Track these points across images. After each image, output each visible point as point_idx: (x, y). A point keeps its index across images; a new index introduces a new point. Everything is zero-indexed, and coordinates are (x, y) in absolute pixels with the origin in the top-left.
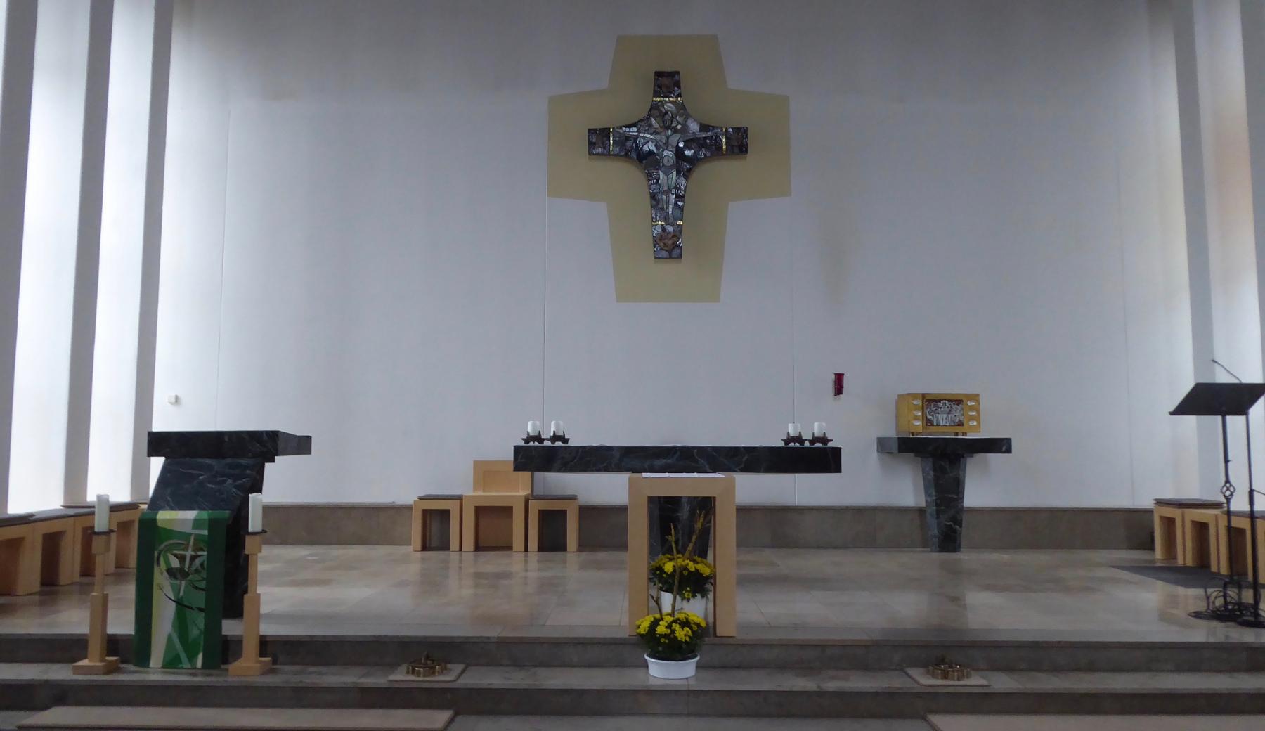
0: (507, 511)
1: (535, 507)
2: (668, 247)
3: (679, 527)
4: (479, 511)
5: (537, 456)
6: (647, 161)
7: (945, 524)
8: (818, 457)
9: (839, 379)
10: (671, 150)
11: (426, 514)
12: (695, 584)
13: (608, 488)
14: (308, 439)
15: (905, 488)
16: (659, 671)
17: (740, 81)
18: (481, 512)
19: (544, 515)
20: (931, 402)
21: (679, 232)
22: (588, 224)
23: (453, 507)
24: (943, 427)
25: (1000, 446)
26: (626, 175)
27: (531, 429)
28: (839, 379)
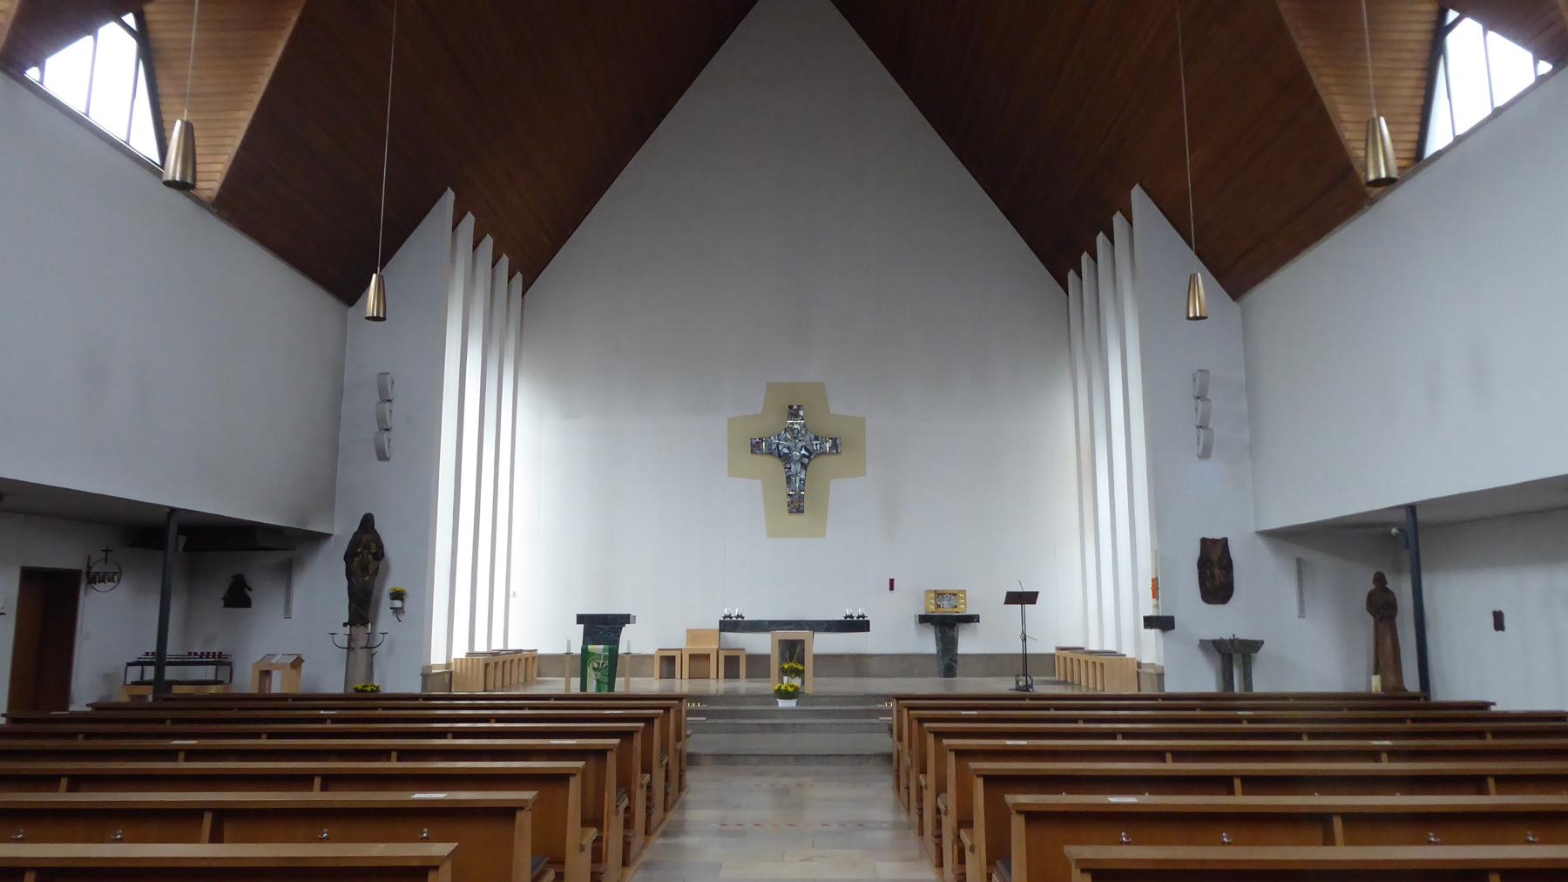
2: (796, 506)
3: (792, 650)
4: (691, 656)
5: (728, 625)
6: (785, 459)
7: (948, 660)
8: (858, 625)
9: (892, 581)
10: (797, 456)
11: (662, 658)
12: (799, 673)
13: (761, 644)
14: (1146, 626)
15: (927, 644)
17: (839, 407)
18: (694, 657)
19: (726, 658)
20: (939, 595)
21: (801, 498)
22: (752, 494)
23: (677, 655)
24: (947, 609)
25: (972, 619)
26: (775, 465)
27: (726, 612)
28: (892, 581)
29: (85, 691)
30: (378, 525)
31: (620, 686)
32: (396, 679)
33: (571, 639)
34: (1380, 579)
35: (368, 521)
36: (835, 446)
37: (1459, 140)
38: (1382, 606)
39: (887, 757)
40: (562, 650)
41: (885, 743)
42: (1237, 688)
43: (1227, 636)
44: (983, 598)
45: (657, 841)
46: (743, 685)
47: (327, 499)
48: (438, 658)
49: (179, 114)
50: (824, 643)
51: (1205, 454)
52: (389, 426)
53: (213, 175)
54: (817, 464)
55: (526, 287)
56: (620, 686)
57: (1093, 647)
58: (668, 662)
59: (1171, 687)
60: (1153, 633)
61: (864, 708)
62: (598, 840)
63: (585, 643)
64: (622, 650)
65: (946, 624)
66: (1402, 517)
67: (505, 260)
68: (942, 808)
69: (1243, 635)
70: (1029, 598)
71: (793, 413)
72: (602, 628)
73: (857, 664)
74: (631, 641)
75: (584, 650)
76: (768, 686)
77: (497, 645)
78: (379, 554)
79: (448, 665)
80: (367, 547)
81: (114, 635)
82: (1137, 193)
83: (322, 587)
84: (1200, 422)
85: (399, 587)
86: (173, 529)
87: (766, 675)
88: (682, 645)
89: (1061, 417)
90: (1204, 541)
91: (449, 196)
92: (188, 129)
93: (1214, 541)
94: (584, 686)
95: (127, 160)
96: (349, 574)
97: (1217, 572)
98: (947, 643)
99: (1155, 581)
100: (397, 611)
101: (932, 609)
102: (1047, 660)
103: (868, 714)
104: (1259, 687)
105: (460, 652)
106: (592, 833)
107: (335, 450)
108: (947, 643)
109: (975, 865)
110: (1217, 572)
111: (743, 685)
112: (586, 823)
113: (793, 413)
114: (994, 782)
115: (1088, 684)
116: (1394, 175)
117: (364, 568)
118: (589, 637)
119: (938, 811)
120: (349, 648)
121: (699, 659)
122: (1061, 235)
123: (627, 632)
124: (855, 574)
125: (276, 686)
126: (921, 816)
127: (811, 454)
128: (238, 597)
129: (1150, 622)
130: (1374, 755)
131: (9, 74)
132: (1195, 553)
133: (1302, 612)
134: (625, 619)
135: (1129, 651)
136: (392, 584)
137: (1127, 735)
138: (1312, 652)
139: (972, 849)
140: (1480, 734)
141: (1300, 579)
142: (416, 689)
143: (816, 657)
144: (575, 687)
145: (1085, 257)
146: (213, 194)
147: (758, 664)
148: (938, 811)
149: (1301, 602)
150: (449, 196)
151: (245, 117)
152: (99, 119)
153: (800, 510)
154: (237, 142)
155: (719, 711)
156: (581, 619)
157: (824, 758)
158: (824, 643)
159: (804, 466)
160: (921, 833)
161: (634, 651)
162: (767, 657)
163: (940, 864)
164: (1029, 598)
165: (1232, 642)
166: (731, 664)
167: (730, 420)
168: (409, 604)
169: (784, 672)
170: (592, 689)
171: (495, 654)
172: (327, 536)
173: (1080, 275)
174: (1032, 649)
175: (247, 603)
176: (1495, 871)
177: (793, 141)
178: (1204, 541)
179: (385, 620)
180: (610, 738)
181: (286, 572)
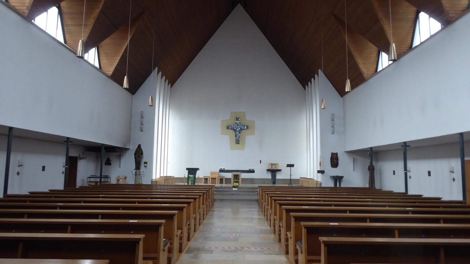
0: (215, 178)
1: (219, 178)
2: (238, 142)
3: (236, 177)
5: (221, 171)
6: (235, 131)
7: (274, 180)
8: (252, 171)
9: (394, 174)
10: (238, 130)
12: (238, 182)
13: (229, 175)
15: (269, 176)
16: (234, 189)
17: (249, 118)
19: (220, 179)
20: (272, 164)
22: (226, 139)
24: (274, 168)
25: (280, 170)
26: (232, 132)
28: (394, 174)
29: (79, 184)
30: (142, 147)
31: (196, 184)
32: (146, 181)
33: (185, 174)
34: (371, 163)
35: (139, 146)
36: (247, 128)
37: (422, 43)
38: (371, 169)
39: (257, 200)
40: (183, 177)
41: (257, 197)
42: (338, 186)
43: (336, 175)
44: (282, 165)
45: (210, 212)
46: (224, 185)
47: (129, 139)
48: (154, 178)
49: (81, 39)
50: (243, 176)
51: (333, 133)
52: (141, 124)
53: (110, 70)
54: (243, 131)
55: (171, 87)
56: (196, 184)
57: (309, 177)
58: (206, 179)
59: (323, 186)
60: (320, 174)
61: (253, 190)
62: (182, 233)
63: (188, 175)
64: (197, 177)
65: (274, 171)
66: (369, 149)
67: (167, 81)
68: (281, 226)
69: (339, 175)
70: (292, 166)
71: (237, 119)
72: (192, 171)
73: (252, 181)
74: (199, 174)
75: (188, 176)
76: (231, 185)
77: (165, 175)
78: (142, 154)
79: (156, 179)
80: (139, 152)
81: (86, 171)
82: (320, 71)
83: (128, 161)
84: (331, 126)
85: (146, 161)
86: (103, 148)
87: (230, 183)
88: (209, 176)
89: (303, 121)
90: (332, 153)
91: (157, 68)
92: (152, 97)
93: (334, 153)
94: (188, 184)
95: (89, 65)
96: (135, 158)
97: (335, 160)
98: (274, 176)
99: (320, 162)
100: (145, 166)
101: (270, 168)
102: (297, 180)
103: (253, 192)
104: (342, 186)
105: (158, 176)
106: (180, 231)
107: (130, 128)
108: (274, 176)
109: (302, 258)
110: (335, 160)
111: (224, 185)
112: (178, 229)
113: (237, 119)
114: (271, 197)
115: (306, 185)
116: (396, 58)
117: (139, 157)
118: (189, 173)
119: (280, 226)
120: (136, 175)
121: (213, 179)
122: (305, 79)
123: (198, 172)
124: (252, 159)
125: (121, 182)
126: (274, 228)
127: (241, 130)
128: (108, 163)
129: (319, 172)
130: (407, 212)
131: (28, 21)
132: (330, 156)
133: (354, 170)
134: (197, 169)
135: (315, 179)
136: (144, 160)
137: (335, 205)
138: (355, 178)
139: (282, 227)
140: (439, 207)
141: (354, 162)
142: (150, 183)
143: (242, 179)
144: (186, 184)
145: (309, 83)
146: (111, 75)
147: (228, 180)
148: (280, 226)
149: (354, 167)
150: (157, 68)
151: (118, 58)
152: (48, 31)
153: (238, 143)
154: (117, 64)
155: (219, 190)
156: (187, 169)
157: (243, 200)
158: (243, 176)
159: (240, 133)
160: (275, 233)
161: (200, 177)
162: (230, 179)
163: (287, 253)
164: (292, 166)
165: (337, 176)
166: (221, 180)
167: (222, 121)
168: (148, 165)
169: (235, 182)
170: (190, 184)
171: (166, 177)
172: (129, 149)
173: (311, 83)
174: (293, 178)
175: (110, 164)
176: (368, 218)
177: (239, 44)
178: (332, 153)
179: (142, 168)
180: (192, 200)
181: (120, 157)
